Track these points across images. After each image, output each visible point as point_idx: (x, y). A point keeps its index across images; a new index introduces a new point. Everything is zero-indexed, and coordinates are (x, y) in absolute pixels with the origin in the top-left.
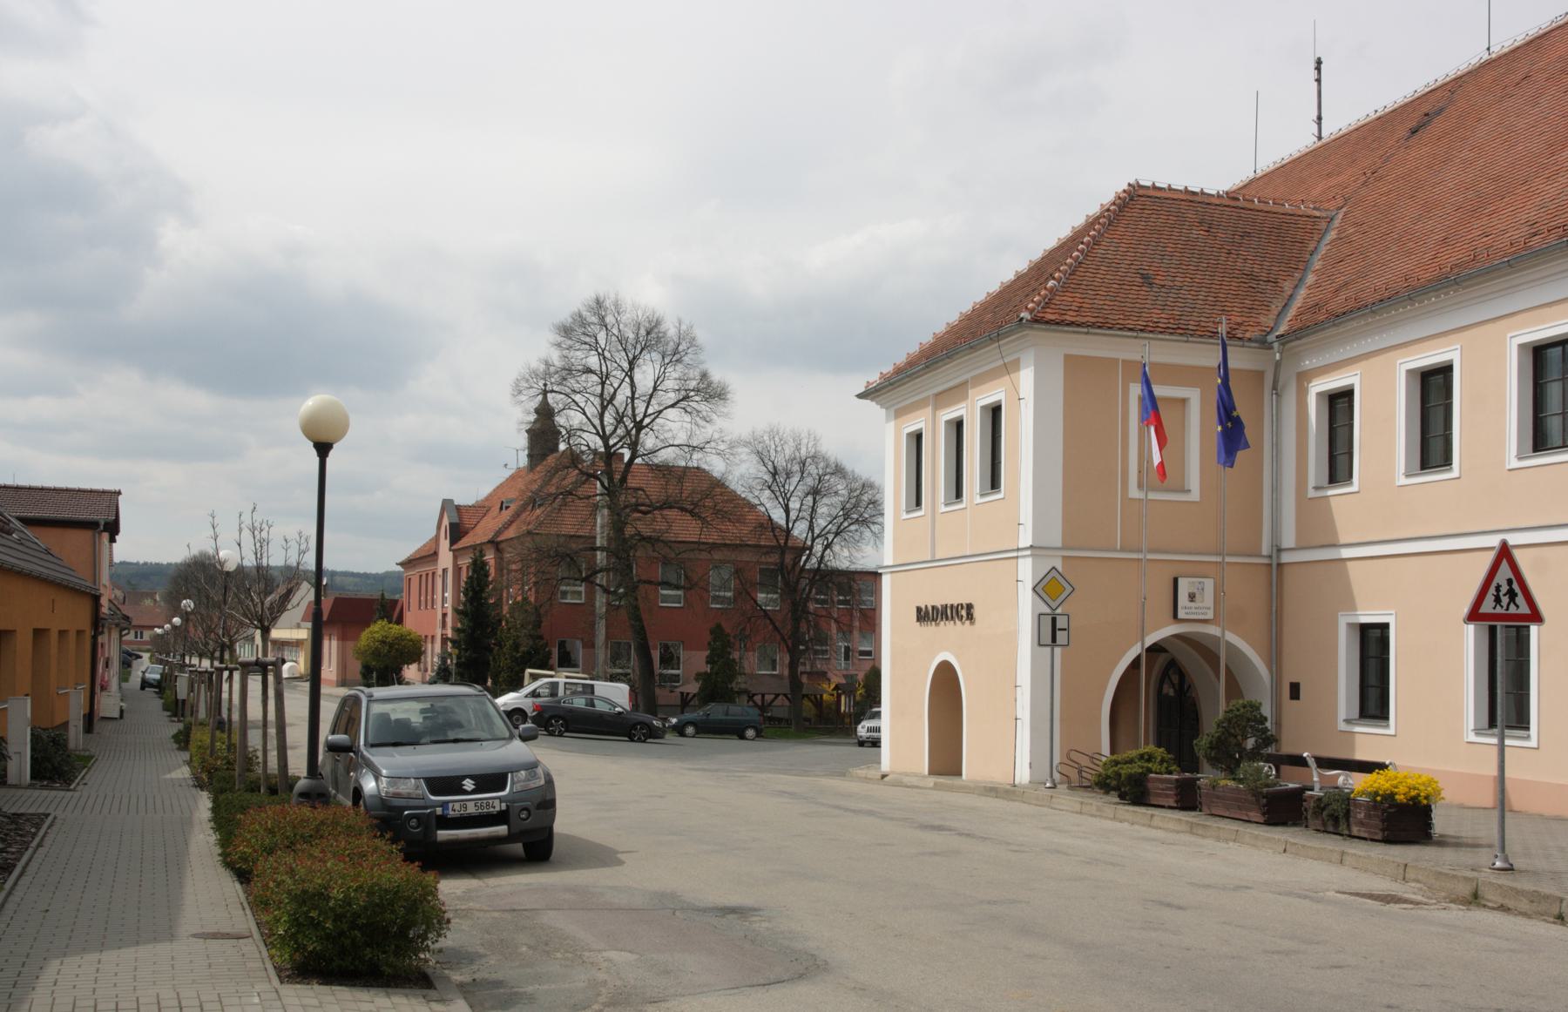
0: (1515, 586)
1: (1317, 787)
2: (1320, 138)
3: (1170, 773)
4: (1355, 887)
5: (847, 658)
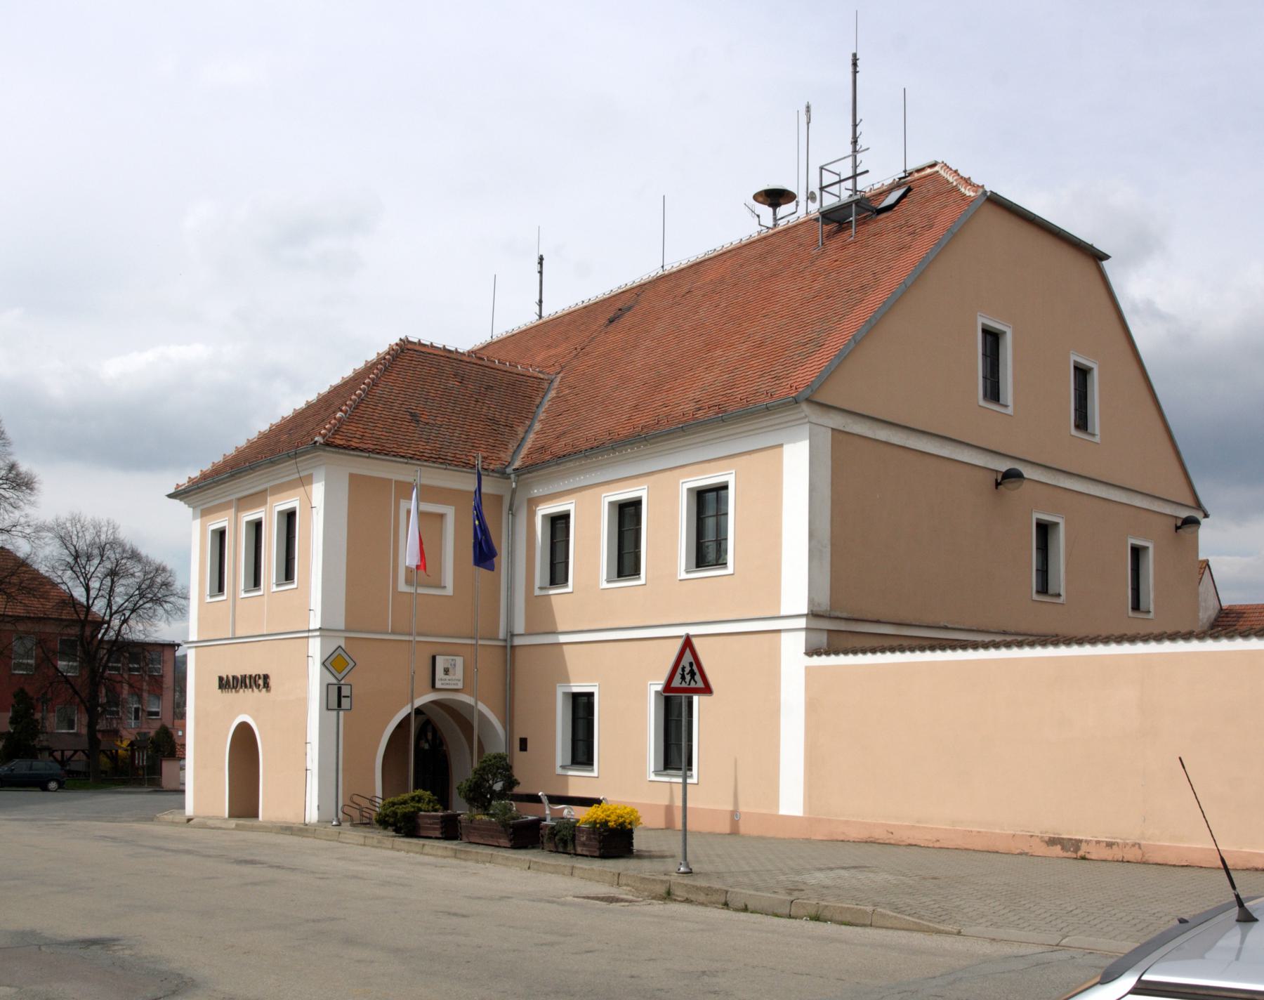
0: (695, 667)
1: (549, 818)
2: (540, 317)
3: (436, 811)
4: (585, 893)
5: (137, 718)
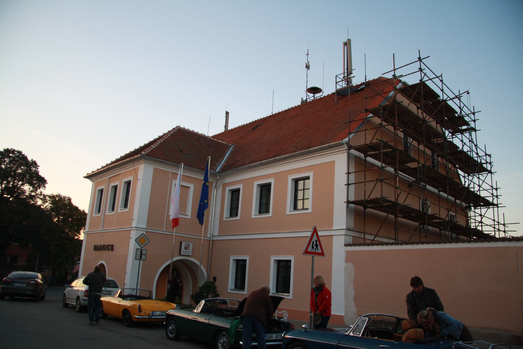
0: (318, 243)
